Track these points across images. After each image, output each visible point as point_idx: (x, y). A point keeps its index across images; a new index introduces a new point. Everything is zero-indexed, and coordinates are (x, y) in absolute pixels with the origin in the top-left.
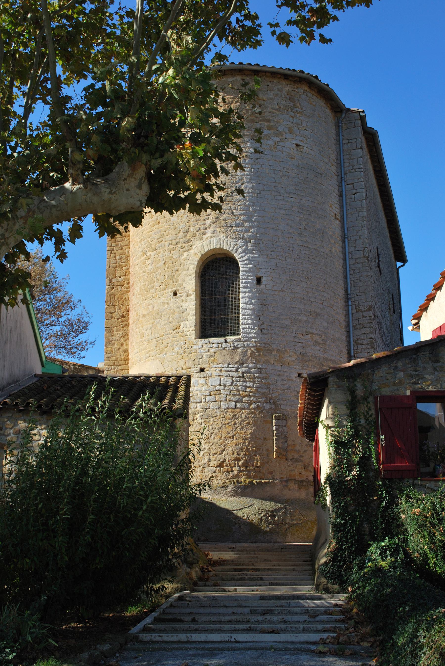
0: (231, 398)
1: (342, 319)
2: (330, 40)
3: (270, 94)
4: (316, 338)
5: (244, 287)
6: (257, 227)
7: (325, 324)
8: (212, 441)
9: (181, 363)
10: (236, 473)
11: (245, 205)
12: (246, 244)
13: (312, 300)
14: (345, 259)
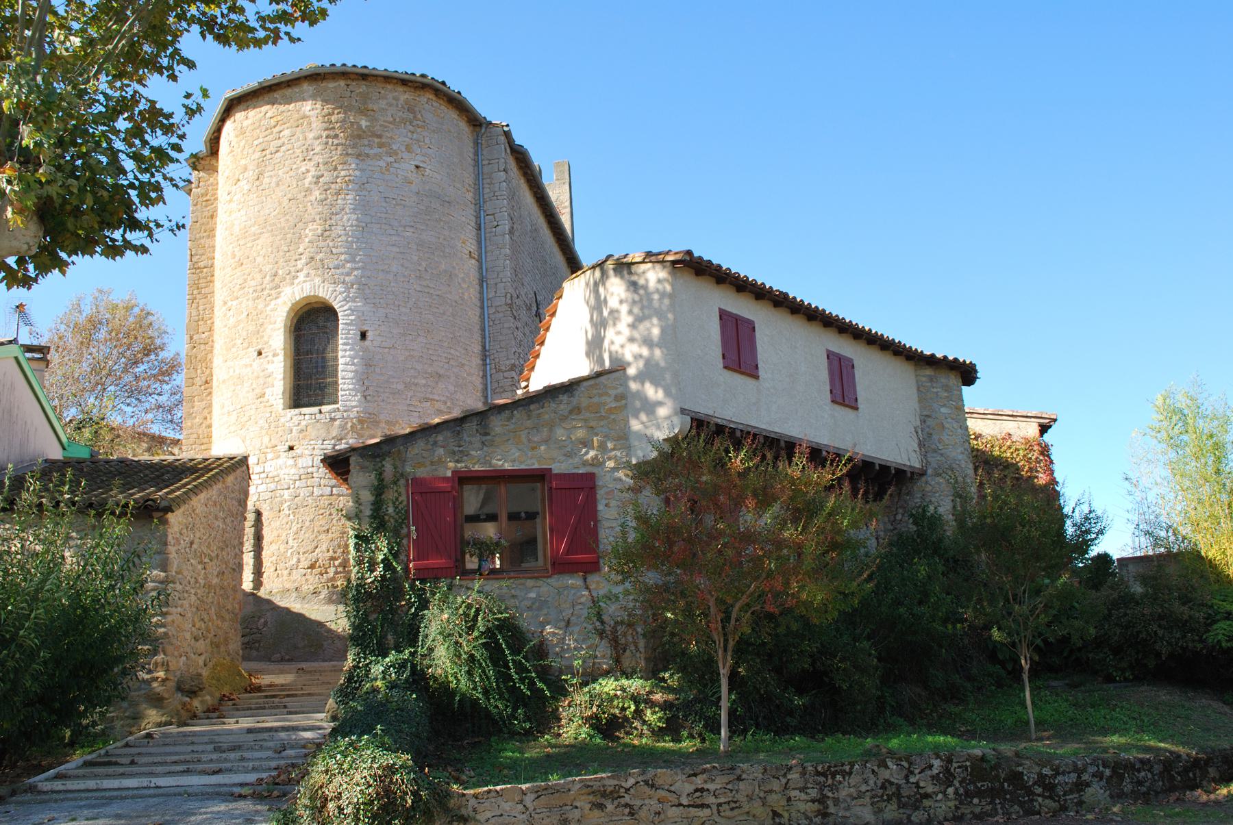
0: (326, 482)
1: (478, 381)
2: (299, 39)
3: (383, 104)
4: (438, 405)
5: (344, 344)
6: (363, 268)
7: (451, 388)
8: (302, 537)
9: (266, 439)
10: (331, 575)
11: (347, 241)
12: (347, 290)
13: (434, 358)
14: (482, 308)
